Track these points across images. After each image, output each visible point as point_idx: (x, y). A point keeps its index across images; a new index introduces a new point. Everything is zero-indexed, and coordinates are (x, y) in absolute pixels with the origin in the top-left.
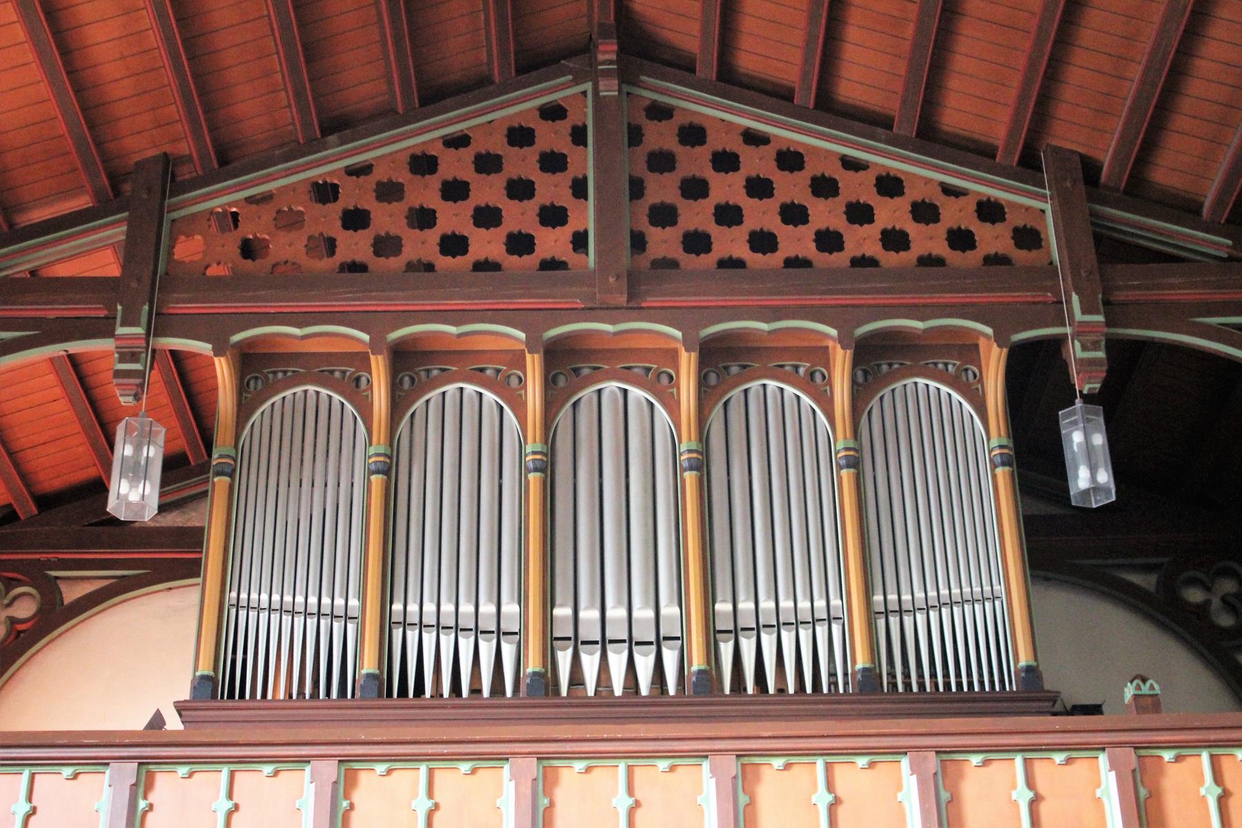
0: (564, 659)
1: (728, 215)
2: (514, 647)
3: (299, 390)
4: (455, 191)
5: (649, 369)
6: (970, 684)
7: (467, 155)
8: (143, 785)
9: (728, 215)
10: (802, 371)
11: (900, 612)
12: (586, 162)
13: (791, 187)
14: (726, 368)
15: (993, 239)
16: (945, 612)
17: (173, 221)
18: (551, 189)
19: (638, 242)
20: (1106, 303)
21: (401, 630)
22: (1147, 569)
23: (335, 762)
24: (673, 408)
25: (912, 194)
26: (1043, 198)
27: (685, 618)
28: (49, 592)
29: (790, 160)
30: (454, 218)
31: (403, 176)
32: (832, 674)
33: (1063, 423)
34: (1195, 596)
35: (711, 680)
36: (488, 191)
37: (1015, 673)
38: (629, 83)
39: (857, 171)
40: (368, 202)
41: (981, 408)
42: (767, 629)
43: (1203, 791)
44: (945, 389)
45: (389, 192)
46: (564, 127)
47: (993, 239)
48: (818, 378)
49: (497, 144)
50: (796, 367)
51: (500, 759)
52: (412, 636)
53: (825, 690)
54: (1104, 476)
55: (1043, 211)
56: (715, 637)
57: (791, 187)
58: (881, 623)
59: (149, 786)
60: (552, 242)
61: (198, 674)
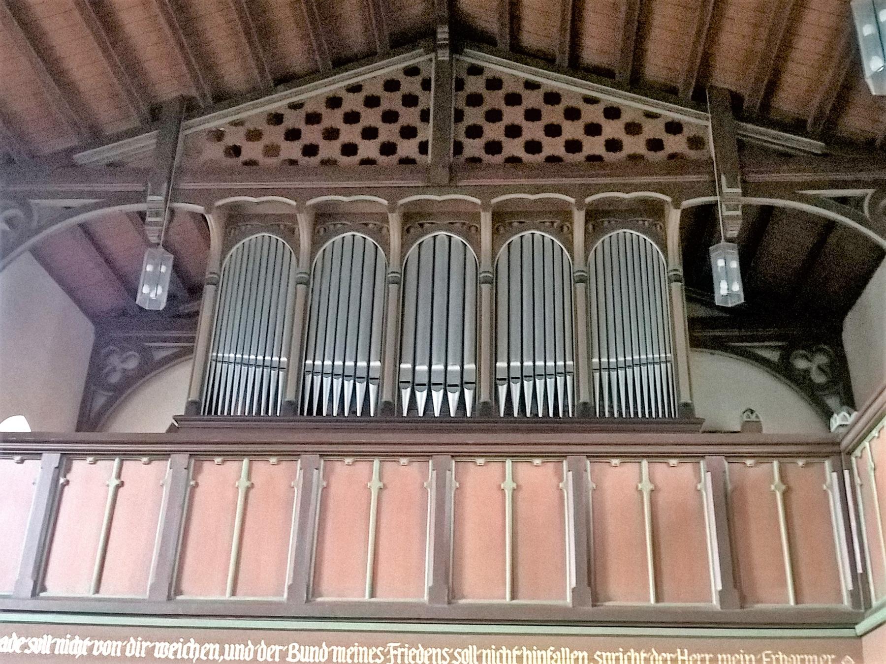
0: (406, 394)
1: (513, 131)
2: (472, 392)
3: (259, 235)
4: (352, 118)
5: (464, 224)
6: (650, 413)
7: (360, 97)
8: (63, 468)
9: (513, 131)
10: (555, 225)
11: (609, 369)
12: (428, 100)
13: (553, 114)
14: (511, 223)
15: (675, 144)
16: (636, 369)
17: (186, 136)
18: (409, 116)
19: (459, 148)
20: (744, 182)
21: (310, 376)
22: (774, 348)
23: (187, 455)
24: (477, 246)
25: (626, 117)
26: (707, 119)
27: (478, 370)
28: (145, 353)
29: (553, 98)
30: (350, 134)
31: (323, 110)
32: (565, 406)
33: (713, 255)
34: (801, 364)
35: (490, 408)
36: (371, 118)
37: (678, 406)
38: (457, 53)
39: (592, 103)
40: (301, 125)
41: (664, 248)
42: (528, 378)
43: (773, 487)
44: (642, 236)
45: (313, 119)
46: (418, 79)
47: (675, 144)
48: (565, 229)
49: (377, 89)
50: (552, 223)
51: (296, 455)
52: (317, 379)
53: (561, 415)
54: (737, 287)
55: (707, 126)
56: (495, 382)
57: (553, 114)
58: (597, 375)
59: (68, 470)
60: (408, 148)
61: (190, 400)
